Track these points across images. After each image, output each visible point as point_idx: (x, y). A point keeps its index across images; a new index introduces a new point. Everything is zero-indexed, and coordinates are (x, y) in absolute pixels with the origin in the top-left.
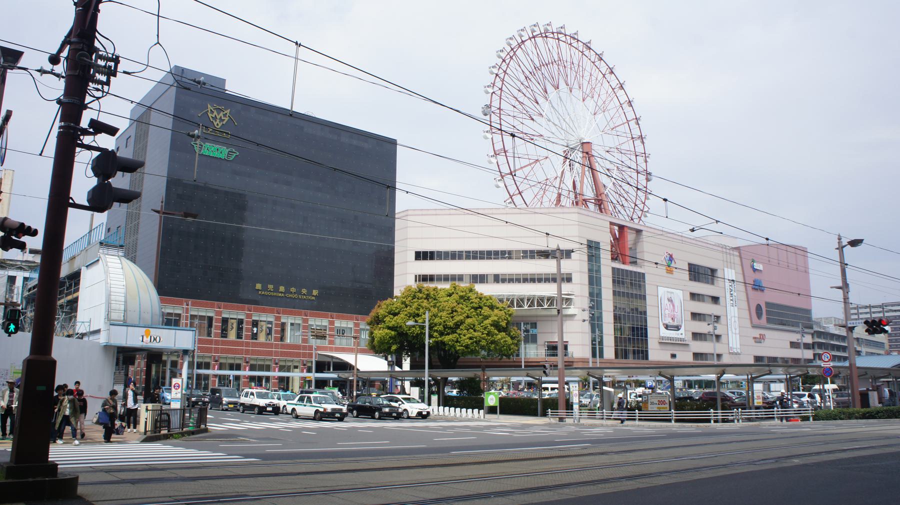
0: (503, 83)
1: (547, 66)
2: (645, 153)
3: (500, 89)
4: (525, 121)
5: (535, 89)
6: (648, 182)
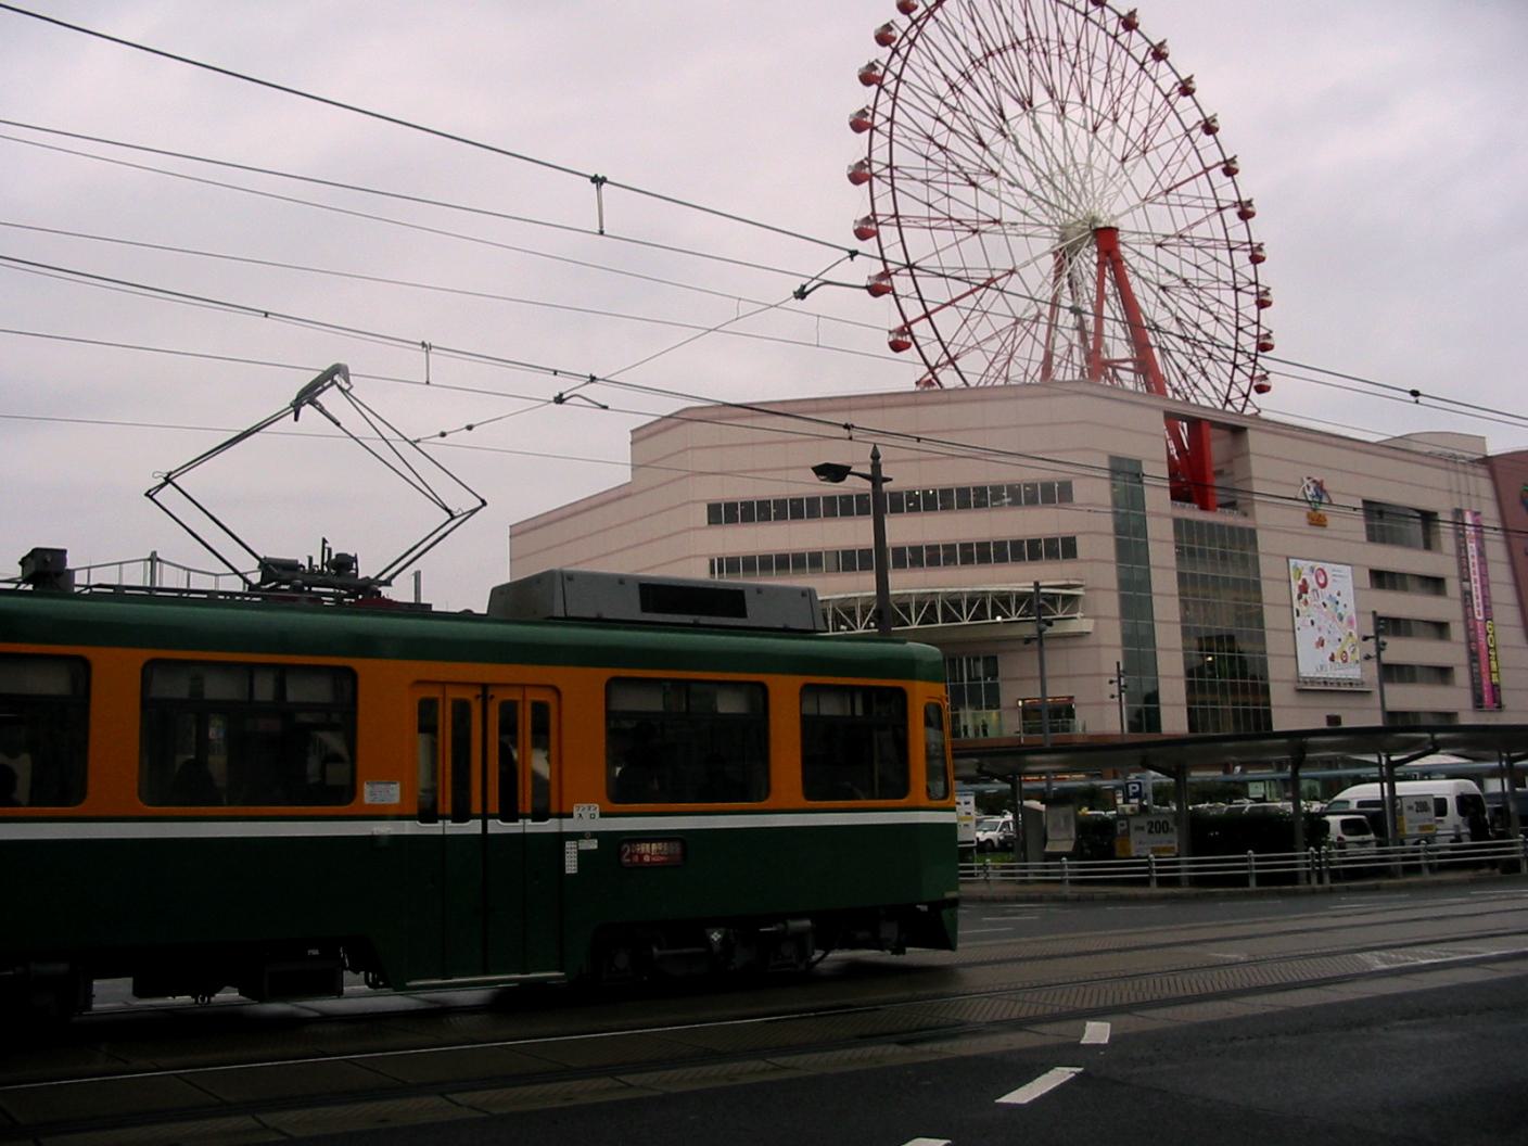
0: (895, 104)
1: (1001, 54)
2: (1250, 242)
3: (888, 119)
4: (953, 191)
5: (975, 113)
6: (1262, 311)
